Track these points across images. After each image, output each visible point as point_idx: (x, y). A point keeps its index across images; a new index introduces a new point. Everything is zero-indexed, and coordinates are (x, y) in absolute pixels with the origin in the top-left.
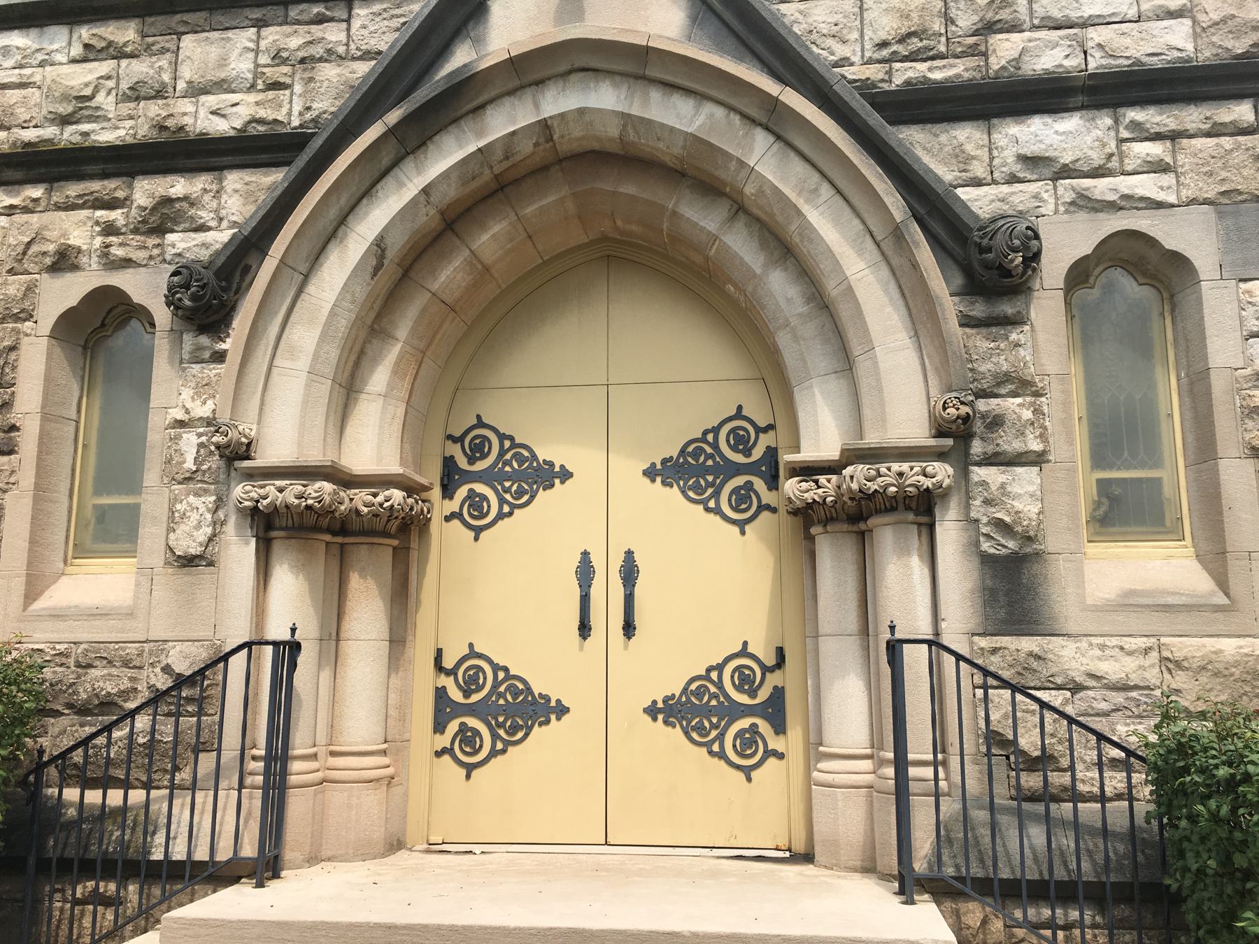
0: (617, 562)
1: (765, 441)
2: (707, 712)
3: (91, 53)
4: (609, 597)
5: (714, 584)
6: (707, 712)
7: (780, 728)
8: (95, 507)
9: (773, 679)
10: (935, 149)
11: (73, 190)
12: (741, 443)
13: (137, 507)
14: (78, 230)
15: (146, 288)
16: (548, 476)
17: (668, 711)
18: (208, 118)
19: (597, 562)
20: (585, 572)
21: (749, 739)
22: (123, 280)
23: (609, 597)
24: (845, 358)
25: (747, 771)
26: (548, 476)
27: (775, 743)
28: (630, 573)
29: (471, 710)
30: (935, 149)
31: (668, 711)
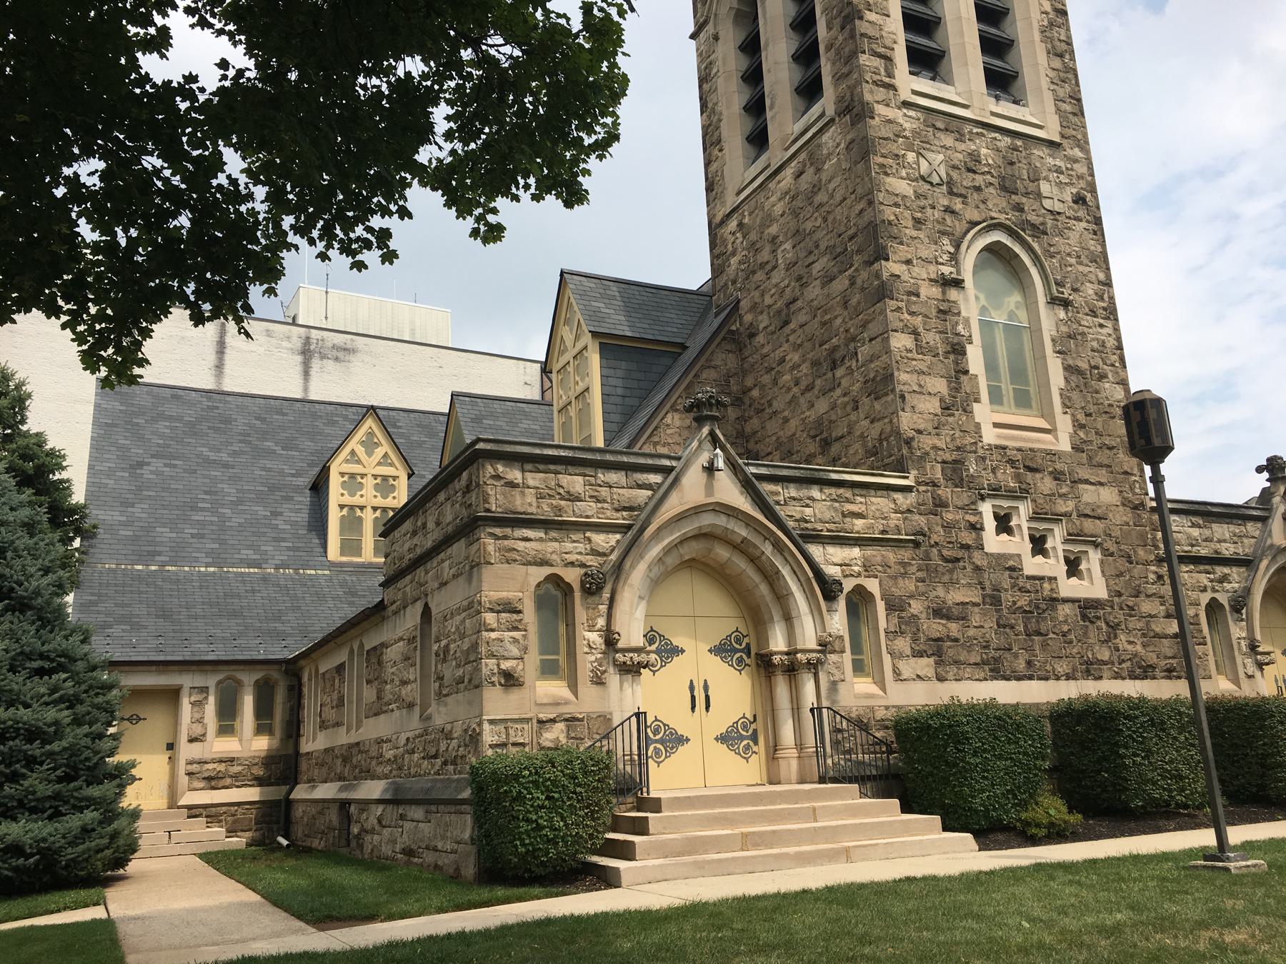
0: (702, 684)
1: (746, 640)
2: (734, 739)
3: (1193, 525)
4: (699, 698)
5: (734, 692)
6: (734, 739)
7: (756, 743)
8: (558, 654)
9: (753, 726)
10: (815, 551)
11: (1202, 567)
12: (738, 641)
13: (541, 654)
14: (1204, 579)
15: (1223, 599)
16: (678, 651)
17: (723, 739)
18: (1227, 550)
19: (695, 684)
20: (692, 688)
21: (747, 747)
22: (1216, 595)
23: (699, 698)
24: (788, 619)
25: (747, 759)
26: (678, 651)
27: (755, 749)
28: (706, 688)
29: (656, 741)
30: (815, 551)
31: (723, 739)
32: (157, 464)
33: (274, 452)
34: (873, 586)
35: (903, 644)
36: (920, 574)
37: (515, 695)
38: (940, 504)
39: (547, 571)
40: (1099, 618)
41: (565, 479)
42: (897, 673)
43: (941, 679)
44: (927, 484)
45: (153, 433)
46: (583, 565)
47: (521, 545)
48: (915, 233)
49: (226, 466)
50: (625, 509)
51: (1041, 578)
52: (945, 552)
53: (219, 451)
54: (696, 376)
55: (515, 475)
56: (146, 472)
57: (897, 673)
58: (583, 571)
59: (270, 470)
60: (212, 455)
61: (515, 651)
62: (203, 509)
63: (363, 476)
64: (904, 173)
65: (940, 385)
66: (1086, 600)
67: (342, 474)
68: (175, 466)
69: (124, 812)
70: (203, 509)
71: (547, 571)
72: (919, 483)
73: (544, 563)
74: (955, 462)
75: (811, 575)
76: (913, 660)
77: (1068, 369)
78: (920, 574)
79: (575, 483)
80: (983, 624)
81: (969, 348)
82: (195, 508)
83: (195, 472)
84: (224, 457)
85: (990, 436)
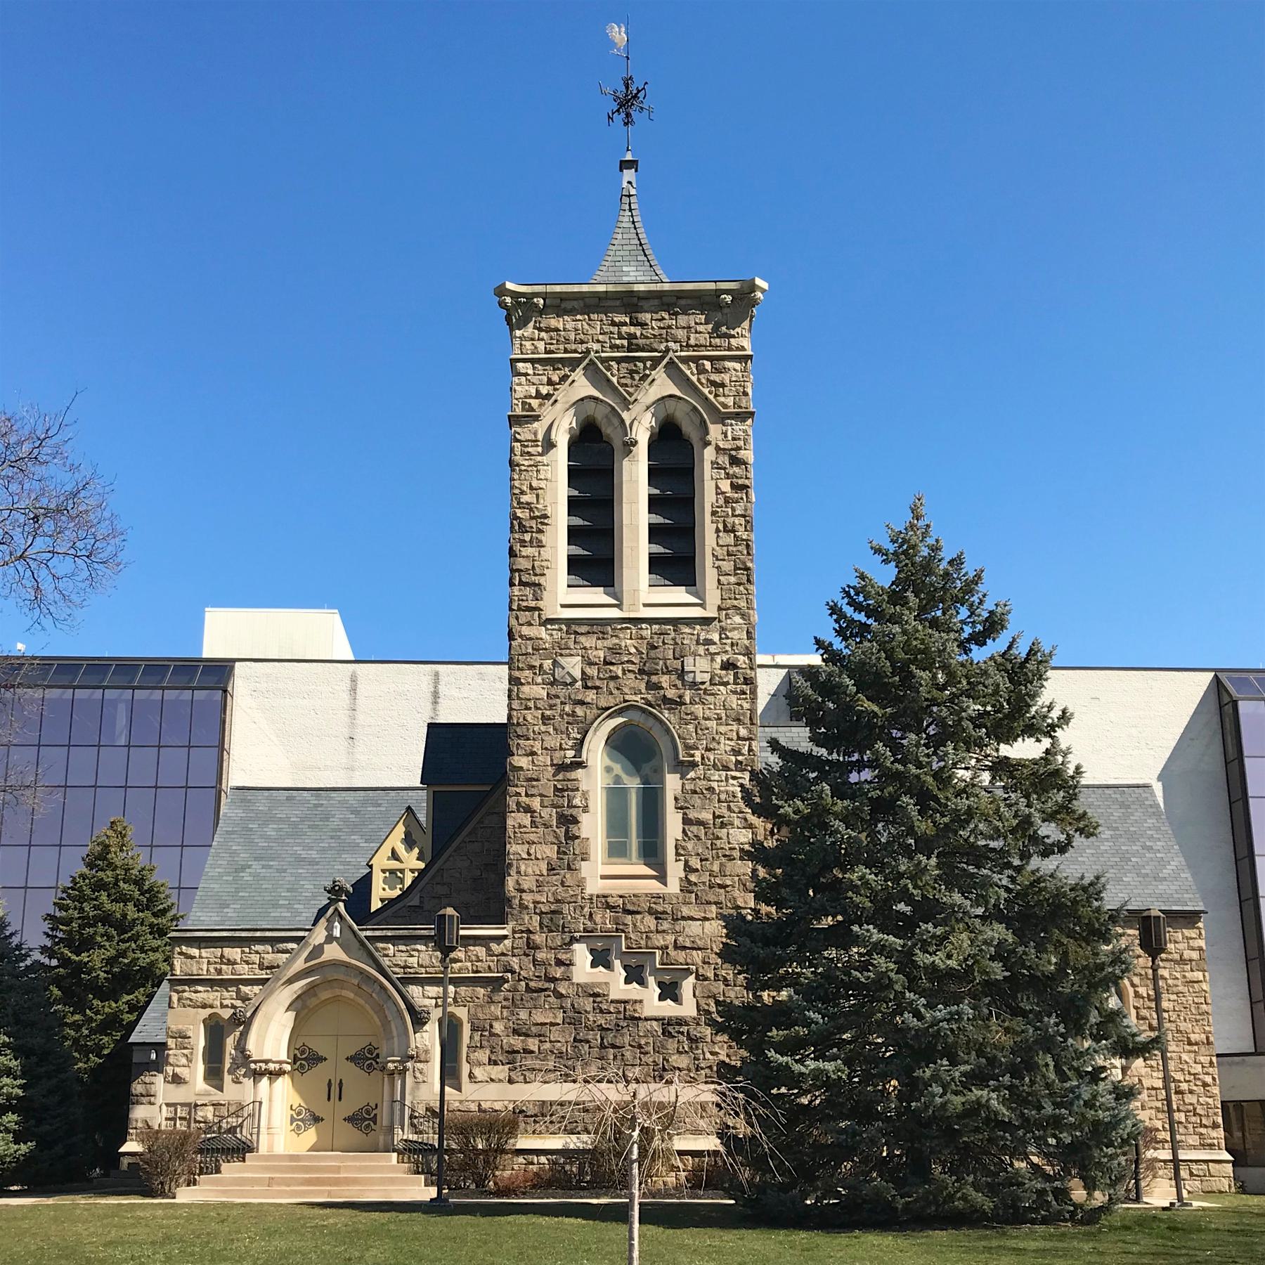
10: (414, 991)
17: (349, 1119)
31: (349, 1119)
32: (256, 866)
33: (357, 845)
34: (462, 1013)
35: (483, 1055)
36: (504, 1003)
37: (183, 1088)
38: (532, 946)
39: (209, 1011)
40: (682, 1033)
41: (227, 951)
42: (471, 1076)
43: (511, 1081)
44: (522, 932)
45: (261, 837)
46: (233, 1007)
47: (194, 996)
48: (543, 728)
49: (313, 862)
50: (268, 968)
51: (625, 1002)
52: (532, 984)
53: (311, 848)
54: (480, 822)
55: (194, 952)
56: (246, 876)
57: (471, 1076)
58: (232, 1011)
59: (349, 863)
60: (304, 854)
61: (184, 1061)
62: (282, 906)
63: (402, 871)
64: (539, 680)
65: (551, 852)
66: (670, 1019)
67: (384, 871)
68: (270, 867)
69: (432, 1184)
70: (282, 906)
71: (209, 1011)
72: (514, 932)
73: (204, 1006)
74: (553, 912)
75: (403, 1006)
76: (488, 1068)
77: (686, 821)
78: (504, 1003)
79: (234, 953)
80: (562, 1038)
81: (584, 818)
82: (276, 906)
83: (285, 871)
84: (314, 854)
85: (594, 886)
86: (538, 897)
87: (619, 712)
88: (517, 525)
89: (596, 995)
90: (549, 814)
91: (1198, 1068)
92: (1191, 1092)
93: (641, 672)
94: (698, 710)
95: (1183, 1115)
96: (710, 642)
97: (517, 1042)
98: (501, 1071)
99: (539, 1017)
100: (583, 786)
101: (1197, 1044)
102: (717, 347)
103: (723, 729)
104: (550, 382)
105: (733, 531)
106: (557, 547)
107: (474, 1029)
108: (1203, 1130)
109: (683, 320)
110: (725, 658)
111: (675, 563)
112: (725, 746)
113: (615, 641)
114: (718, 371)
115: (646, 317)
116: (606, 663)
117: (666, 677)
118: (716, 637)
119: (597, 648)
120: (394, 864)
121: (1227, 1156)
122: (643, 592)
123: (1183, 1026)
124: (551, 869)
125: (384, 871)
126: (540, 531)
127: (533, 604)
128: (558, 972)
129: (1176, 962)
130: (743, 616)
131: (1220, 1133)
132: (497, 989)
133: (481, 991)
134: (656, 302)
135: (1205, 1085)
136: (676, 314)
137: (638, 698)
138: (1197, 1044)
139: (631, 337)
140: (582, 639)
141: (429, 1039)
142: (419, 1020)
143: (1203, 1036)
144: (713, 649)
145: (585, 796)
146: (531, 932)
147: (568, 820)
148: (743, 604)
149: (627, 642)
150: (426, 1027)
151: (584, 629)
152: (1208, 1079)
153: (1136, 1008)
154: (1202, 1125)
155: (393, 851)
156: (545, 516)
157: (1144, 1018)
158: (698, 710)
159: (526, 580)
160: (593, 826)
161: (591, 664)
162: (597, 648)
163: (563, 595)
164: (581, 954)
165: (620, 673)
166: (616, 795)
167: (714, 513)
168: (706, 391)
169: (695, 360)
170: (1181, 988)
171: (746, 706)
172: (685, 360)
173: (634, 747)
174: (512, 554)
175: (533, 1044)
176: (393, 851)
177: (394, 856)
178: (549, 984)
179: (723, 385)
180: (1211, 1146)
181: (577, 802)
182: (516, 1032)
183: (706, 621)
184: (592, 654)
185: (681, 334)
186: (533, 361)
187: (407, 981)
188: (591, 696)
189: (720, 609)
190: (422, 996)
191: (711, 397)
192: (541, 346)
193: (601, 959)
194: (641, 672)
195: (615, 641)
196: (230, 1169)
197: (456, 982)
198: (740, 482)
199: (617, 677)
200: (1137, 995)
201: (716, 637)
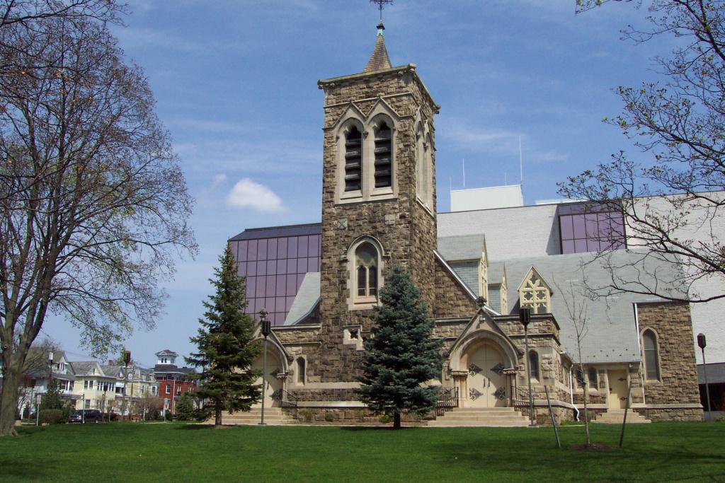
34: (305, 357)
35: (312, 372)
42: (308, 380)
43: (322, 382)
64: (332, 229)
65: (336, 295)
75: (512, 347)
80: (339, 366)
81: (348, 281)
85: (352, 307)
86: (331, 313)
87: (361, 239)
88: (326, 170)
89: (352, 349)
90: (336, 280)
91: (688, 368)
92: (685, 379)
93: (370, 222)
94: (391, 235)
95: (681, 389)
96: (395, 208)
97: (323, 367)
98: (318, 378)
99: (331, 358)
100: (348, 269)
101: (687, 358)
102: (398, 92)
103: (399, 242)
104: (338, 115)
105: (404, 163)
106: (341, 176)
107: (309, 363)
108: (690, 395)
109: (385, 84)
110: (401, 213)
111: (383, 179)
112: (401, 249)
113: (360, 211)
114: (399, 101)
115: (371, 84)
116: (357, 220)
117: (379, 223)
118: (397, 206)
119: (353, 214)
120: (529, 289)
121: (701, 406)
122: (371, 190)
123: (681, 350)
124: (336, 301)
125: (524, 292)
126: (333, 171)
127: (330, 199)
128: (338, 341)
129: (678, 322)
130: (407, 196)
131: (699, 396)
132: (318, 347)
133: (311, 348)
134: (376, 78)
135: (691, 375)
136: (383, 81)
137: (368, 232)
138: (687, 358)
139: (367, 92)
140: (348, 212)
141: (295, 366)
142: (290, 361)
143: (690, 354)
144: (396, 211)
145: (348, 273)
146: (328, 326)
147: (343, 282)
148: (407, 192)
149: (365, 212)
150: (293, 363)
151: (348, 208)
152: (693, 373)
153: (660, 343)
154: (690, 393)
155: (528, 284)
156: (335, 166)
157: (663, 348)
158: (391, 235)
159: (328, 191)
160: (353, 284)
161: (351, 221)
162: (353, 214)
163: (342, 195)
164: (347, 334)
165: (361, 223)
166: (362, 270)
167: (397, 157)
168: (393, 110)
169: (390, 98)
170: (680, 334)
171: (409, 232)
172: (386, 99)
173: (366, 250)
174: (324, 181)
175: (328, 368)
176: (528, 284)
177: (528, 286)
178: (335, 343)
179: (400, 107)
180: (694, 402)
181: (345, 275)
182: (324, 363)
183: (395, 200)
184: (352, 217)
185: (384, 89)
186: (331, 107)
187: (285, 346)
188: (351, 233)
189: (399, 194)
190: (292, 351)
191: (396, 112)
192: (334, 101)
193: (354, 335)
194: (370, 222)
195: (360, 211)
196: (447, 414)
197: (531, 337)
198: (406, 143)
199: (360, 225)
200: (660, 338)
201: (397, 206)
